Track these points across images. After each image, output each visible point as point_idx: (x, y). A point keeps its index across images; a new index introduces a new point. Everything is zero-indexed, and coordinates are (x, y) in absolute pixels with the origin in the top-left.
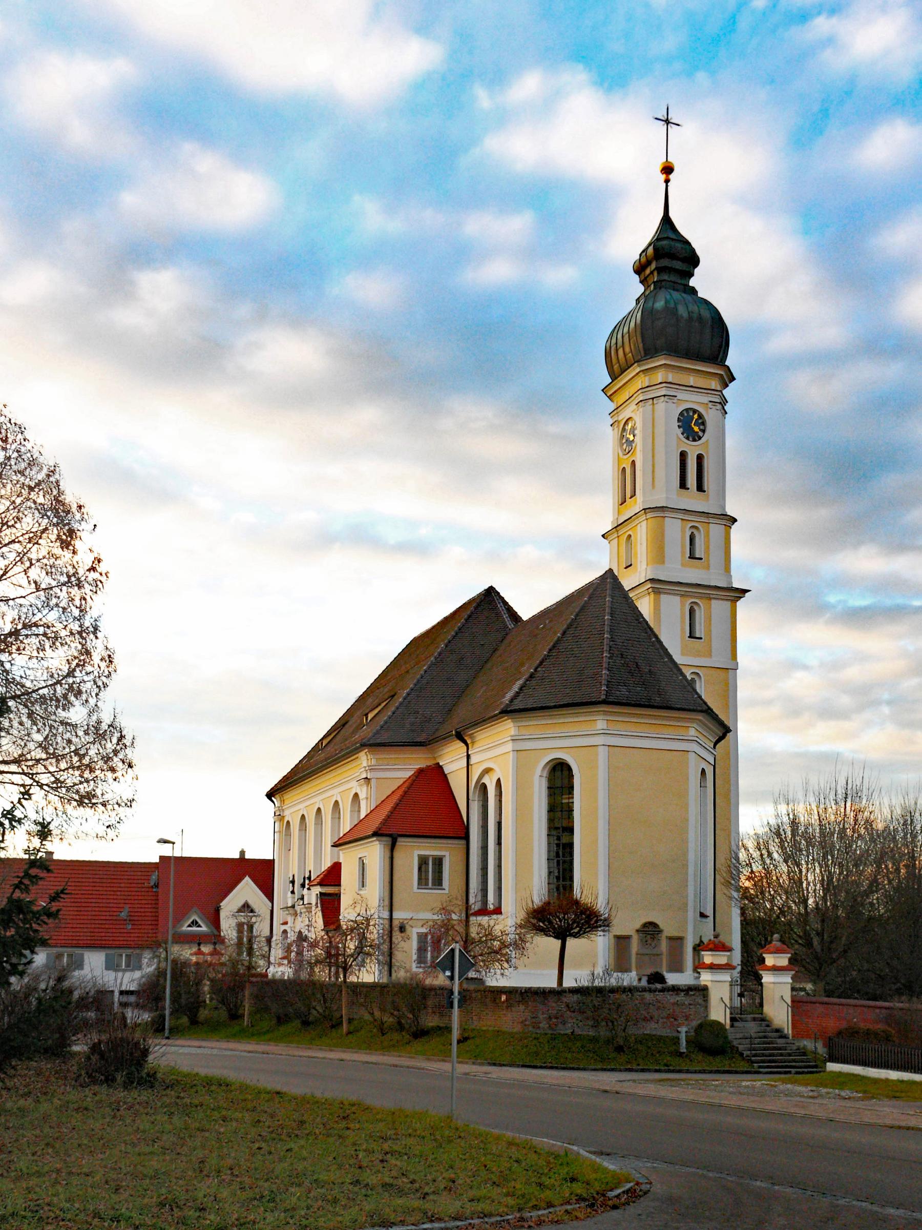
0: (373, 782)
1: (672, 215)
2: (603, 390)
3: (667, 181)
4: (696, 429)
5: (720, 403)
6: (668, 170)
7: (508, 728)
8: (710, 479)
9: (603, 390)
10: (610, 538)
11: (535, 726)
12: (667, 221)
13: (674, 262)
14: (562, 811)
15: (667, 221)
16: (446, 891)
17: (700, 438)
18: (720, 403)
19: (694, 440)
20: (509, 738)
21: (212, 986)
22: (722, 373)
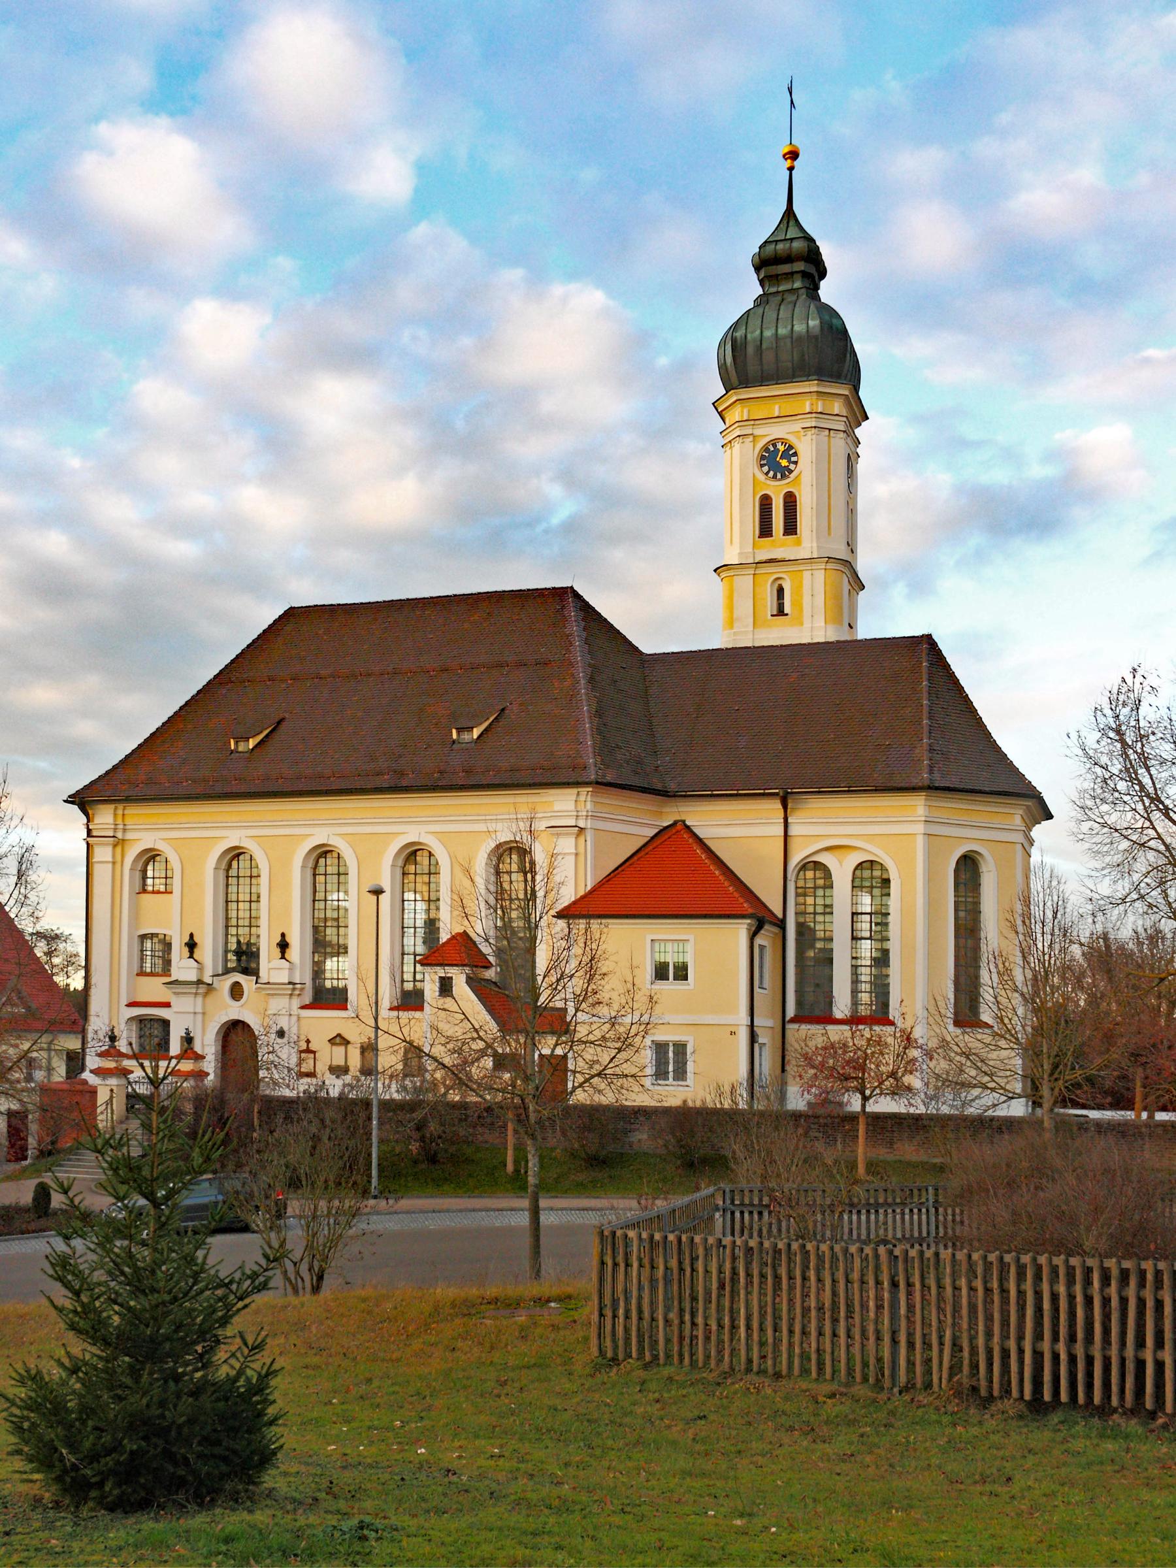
0: (589, 835)
1: (796, 208)
2: (713, 404)
3: (791, 169)
4: (784, 463)
5: (844, 432)
6: (793, 155)
7: (917, 806)
8: (803, 523)
9: (713, 404)
10: (723, 575)
11: (952, 808)
12: (789, 214)
13: (795, 264)
14: (325, 875)
15: (789, 214)
16: (692, 987)
17: (791, 472)
18: (844, 432)
19: (783, 477)
20: (923, 819)
21: (1137, 1127)
22: (846, 392)
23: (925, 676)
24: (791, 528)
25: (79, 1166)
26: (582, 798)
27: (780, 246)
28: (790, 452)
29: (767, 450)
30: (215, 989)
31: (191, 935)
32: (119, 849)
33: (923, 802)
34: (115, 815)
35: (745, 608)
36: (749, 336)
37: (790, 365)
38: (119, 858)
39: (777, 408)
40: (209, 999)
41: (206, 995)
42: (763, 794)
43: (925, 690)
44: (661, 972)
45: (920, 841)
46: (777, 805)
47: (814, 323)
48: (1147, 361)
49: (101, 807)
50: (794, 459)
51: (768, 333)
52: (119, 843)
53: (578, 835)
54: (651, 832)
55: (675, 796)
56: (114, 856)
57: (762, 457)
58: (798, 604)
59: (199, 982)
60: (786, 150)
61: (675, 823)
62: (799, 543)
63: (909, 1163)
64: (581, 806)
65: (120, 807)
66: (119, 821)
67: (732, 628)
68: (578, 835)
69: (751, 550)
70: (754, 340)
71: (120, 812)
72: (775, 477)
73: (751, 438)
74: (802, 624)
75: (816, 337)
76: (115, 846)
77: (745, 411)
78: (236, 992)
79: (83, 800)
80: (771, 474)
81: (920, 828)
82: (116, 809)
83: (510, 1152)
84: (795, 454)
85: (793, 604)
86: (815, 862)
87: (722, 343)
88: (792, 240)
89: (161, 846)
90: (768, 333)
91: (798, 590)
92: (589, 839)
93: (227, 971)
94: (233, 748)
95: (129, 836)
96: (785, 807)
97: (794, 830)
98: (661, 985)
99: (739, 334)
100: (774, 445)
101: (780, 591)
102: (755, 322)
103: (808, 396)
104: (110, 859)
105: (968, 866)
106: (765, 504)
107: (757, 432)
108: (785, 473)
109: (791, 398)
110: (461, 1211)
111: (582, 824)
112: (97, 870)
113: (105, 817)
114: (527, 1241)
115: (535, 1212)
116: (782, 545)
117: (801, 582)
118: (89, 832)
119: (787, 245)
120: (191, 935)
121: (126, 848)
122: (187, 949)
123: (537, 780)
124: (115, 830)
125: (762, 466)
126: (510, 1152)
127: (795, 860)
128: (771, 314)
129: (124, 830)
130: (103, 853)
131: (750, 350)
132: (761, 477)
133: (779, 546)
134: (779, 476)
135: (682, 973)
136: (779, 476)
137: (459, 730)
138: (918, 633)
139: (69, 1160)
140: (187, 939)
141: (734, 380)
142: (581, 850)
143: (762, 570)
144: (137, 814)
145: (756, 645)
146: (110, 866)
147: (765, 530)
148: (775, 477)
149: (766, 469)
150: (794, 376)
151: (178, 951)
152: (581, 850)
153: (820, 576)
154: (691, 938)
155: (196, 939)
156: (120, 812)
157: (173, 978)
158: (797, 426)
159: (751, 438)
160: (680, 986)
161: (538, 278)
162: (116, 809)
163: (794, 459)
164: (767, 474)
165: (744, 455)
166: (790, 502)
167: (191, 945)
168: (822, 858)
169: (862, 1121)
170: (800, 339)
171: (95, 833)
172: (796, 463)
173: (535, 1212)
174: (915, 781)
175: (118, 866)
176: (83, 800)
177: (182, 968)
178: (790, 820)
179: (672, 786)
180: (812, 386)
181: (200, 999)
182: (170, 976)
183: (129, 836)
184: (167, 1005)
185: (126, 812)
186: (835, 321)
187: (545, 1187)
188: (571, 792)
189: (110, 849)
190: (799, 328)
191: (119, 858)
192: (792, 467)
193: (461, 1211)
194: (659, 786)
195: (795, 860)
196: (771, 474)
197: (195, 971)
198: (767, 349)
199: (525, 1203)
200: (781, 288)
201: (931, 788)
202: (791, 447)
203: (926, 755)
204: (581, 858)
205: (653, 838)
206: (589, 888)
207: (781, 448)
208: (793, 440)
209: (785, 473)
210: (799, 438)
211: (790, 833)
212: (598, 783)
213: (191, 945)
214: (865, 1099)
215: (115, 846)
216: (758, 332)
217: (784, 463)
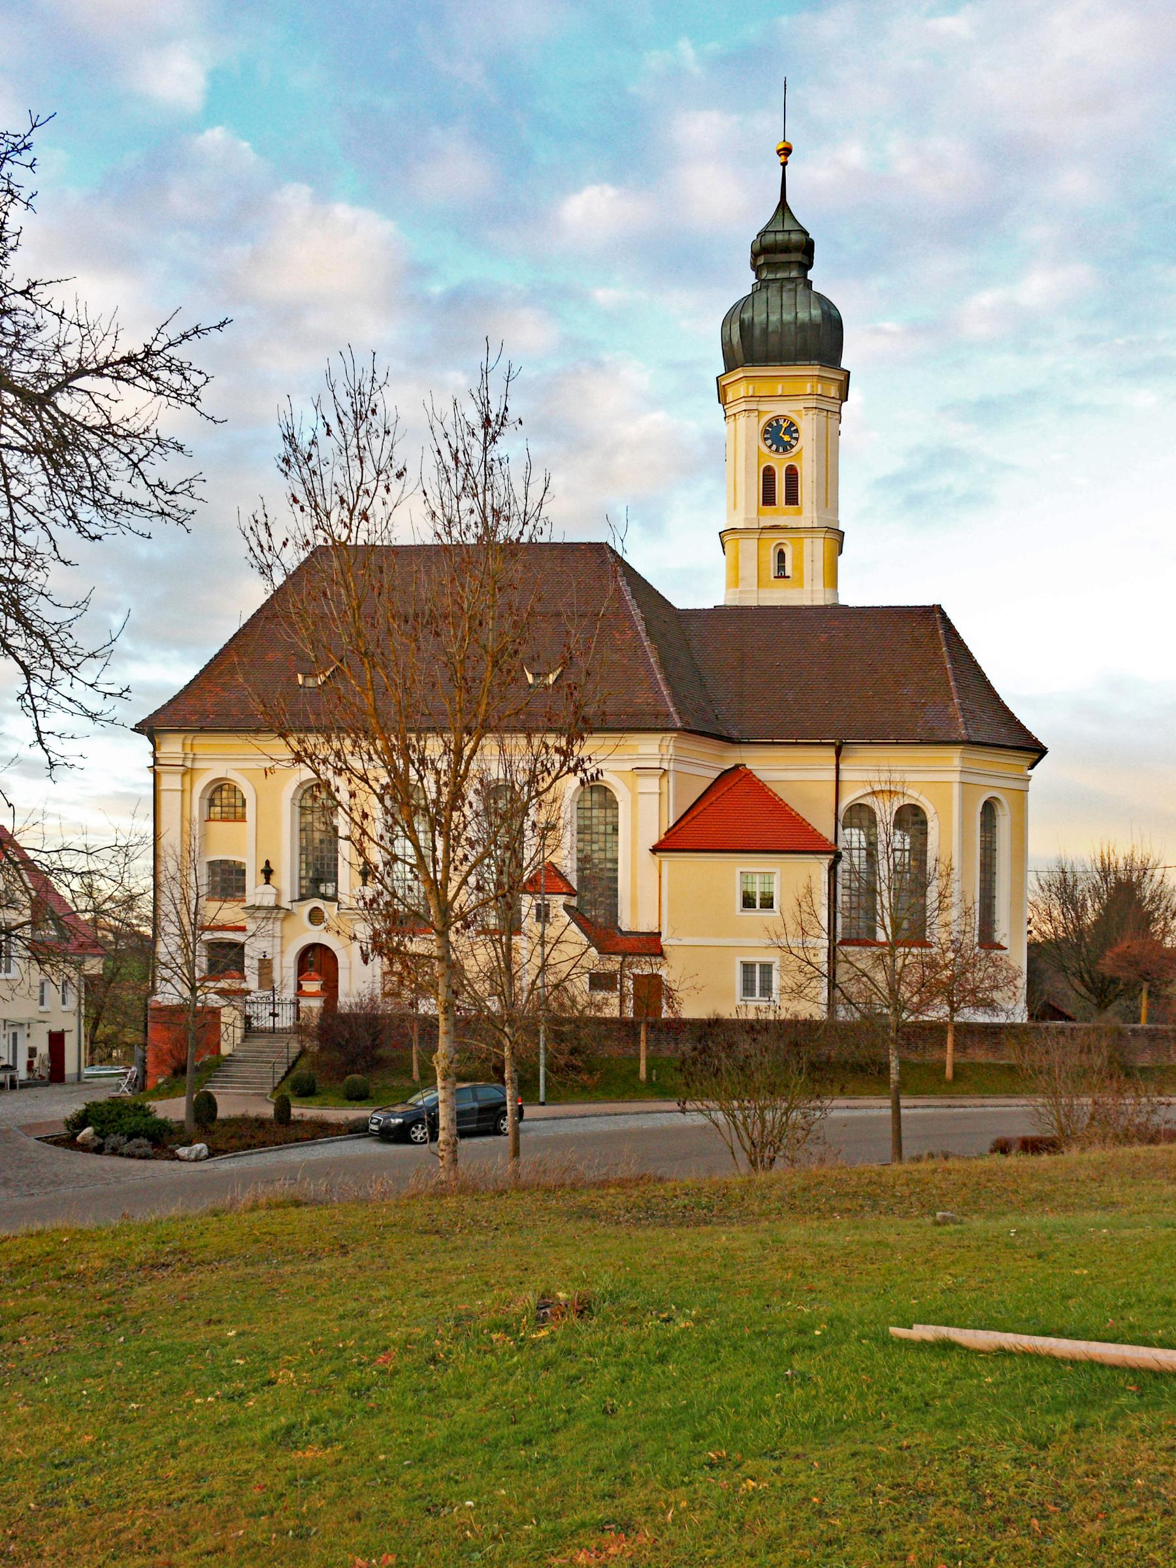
3: (784, 164)
4: (786, 438)
6: (786, 151)
7: (954, 757)
11: (984, 759)
12: (783, 206)
15: (783, 206)
19: (785, 450)
23: (943, 643)
24: (792, 498)
25: (231, 1082)
26: (665, 743)
27: (780, 237)
28: (792, 429)
29: (770, 425)
30: (294, 914)
31: (267, 863)
32: (187, 778)
33: (958, 755)
34: (183, 744)
35: (749, 569)
36: (756, 319)
37: (792, 348)
38: (188, 787)
39: (780, 387)
40: (286, 924)
41: (284, 919)
42: (797, 743)
43: (946, 655)
44: (748, 902)
45: (956, 790)
46: (831, 752)
47: (816, 313)
48: (878, 331)
49: (169, 736)
50: (795, 435)
51: (774, 318)
52: (188, 773)
53: (662, 776)
54: (715, 774)
55: (740, 743)
56: (182, 785)
57: (766, 432)
58: (798, 567)
59: (277, 907)
60: (781, 147)
61: (737, 767)
62: (799, 512)
63: (981, 1065)
64: (664, 750)
65: (191, 736)
66: (188, 750)
67: (737, 586)
68: (662, 776)
69: (755, 516)
70: (761, 323)
71: (189, 742)
72: (777, 450)
73: (756, 413)
74: (802, 586)
75: (818, 326)
76: (184, 775)
77: (751, 387)
78: (316, 916)
79: (149, 728)
80: (774, 447)
81: (956, 777)
82: (185, 739)
83: (643, 1062)
84: (796, 431)
85: (794, 568)
86: (860, 805)
87: (727, 321)
88: (789, 231)
89: (232, 775)
90: (774, 318)
91: (798, 556)
92: (671, 780)
93: (303, 898)
94: (301, 682)
95: (198, 765)
96: (838, 754)
97: (844, 776)
98: (750, 914)
99: (746, 316)
100: (777, 421)
101: (781, 556)
102: (760, 306)
103: (810, 379)
104: (180, 788)
105: (989, 808)
106: (768, 475)
107: (762, 408)
108: (787, 447)
109: (798, 380)
110: (637, 1113)
111: (665, 766)
112: (164, 798)
113: (173, 746)
114: (888, 1130)
115: (896, 1108)
116: (784, 514)
117: (802, 548)
118: (155, 759)
119: (786, 236)
120: (267, 863)
121: (195, 776)
122: (263, 876)
123: (624, 725)
124: (184, 759)
125: (766, 439)
126: (643, 1062)
127: (845, 803)
128: (775, 301)
129: (194, 760)
130: (171, 782)
131: (757, 332)
132: (765, 450)
133: (781, 514)
134: (781, 450)
135: (768, 903)
136: (781, 450)
137: (536, 675)
138: (929, 603)
139: (216, 1076)
140: (263, 866)
141: (739, 355)
142: (665, 790)
143: (767, 535)
144: (205, 744)
145: (761, 604)
146: (179, 794)
147: (768, 499)
148: (777, 450)
149: (769, 442)
150: (796, 360)
151: (252, 878)
152: (665, 790)
153: (819, 543)
154: (777, 870)
155: (272, 866)
156: (189, 742)
157: (247, 904)
158: (800, 405)
159: (756, 413)
160: (766, 914)
161: (323, 195)
162: (185, 739)
163: (795, 435)
164: (770, 447)
165: (749, 429)
166: (792, 474)
167: (268, 872)
168: (868, 801)
169: (950, 1028)
170: (803, 324)
171: (162, 762)
172: (797, 439)
173: (896, 1108)
174: (954, 736)
175: (187, 795)
176: (149, 728)
177: (256, 892)
178: (841, 767)
179: (735, 733)
180: (815, 370)
181: (278, 924)
182: (244, 901)
183: (198, 765)
184: (243, 929)
185: (195, 742)
186: (833, 312)
187: (903, 1087)
188: (656, 738)
189: (179, 778)
190: (803, 316)
191: (188, 787)
192: (793, 442)
193: (637, 1113)
194: (725, 733)
195: (845, 803)
196: (774, 447)
197: (273, 897)
198: (773, 332)
199: (888, 1103)
200: (779, 276)
201: (968, 743)
202: (792, 424)
203: (960, 714)
204: (665, 797)
205: (716, 780)
206: (671, 824)
207: (785, 425)
208: (794, 417)
209: (787, 447)
210: (800, 417)
211: (841, 778)
212: (685, 730)
213: (268, 872)
214: (954, 1010)
215: (184, 775)
216: (764, 315)
217: (786, 438)
